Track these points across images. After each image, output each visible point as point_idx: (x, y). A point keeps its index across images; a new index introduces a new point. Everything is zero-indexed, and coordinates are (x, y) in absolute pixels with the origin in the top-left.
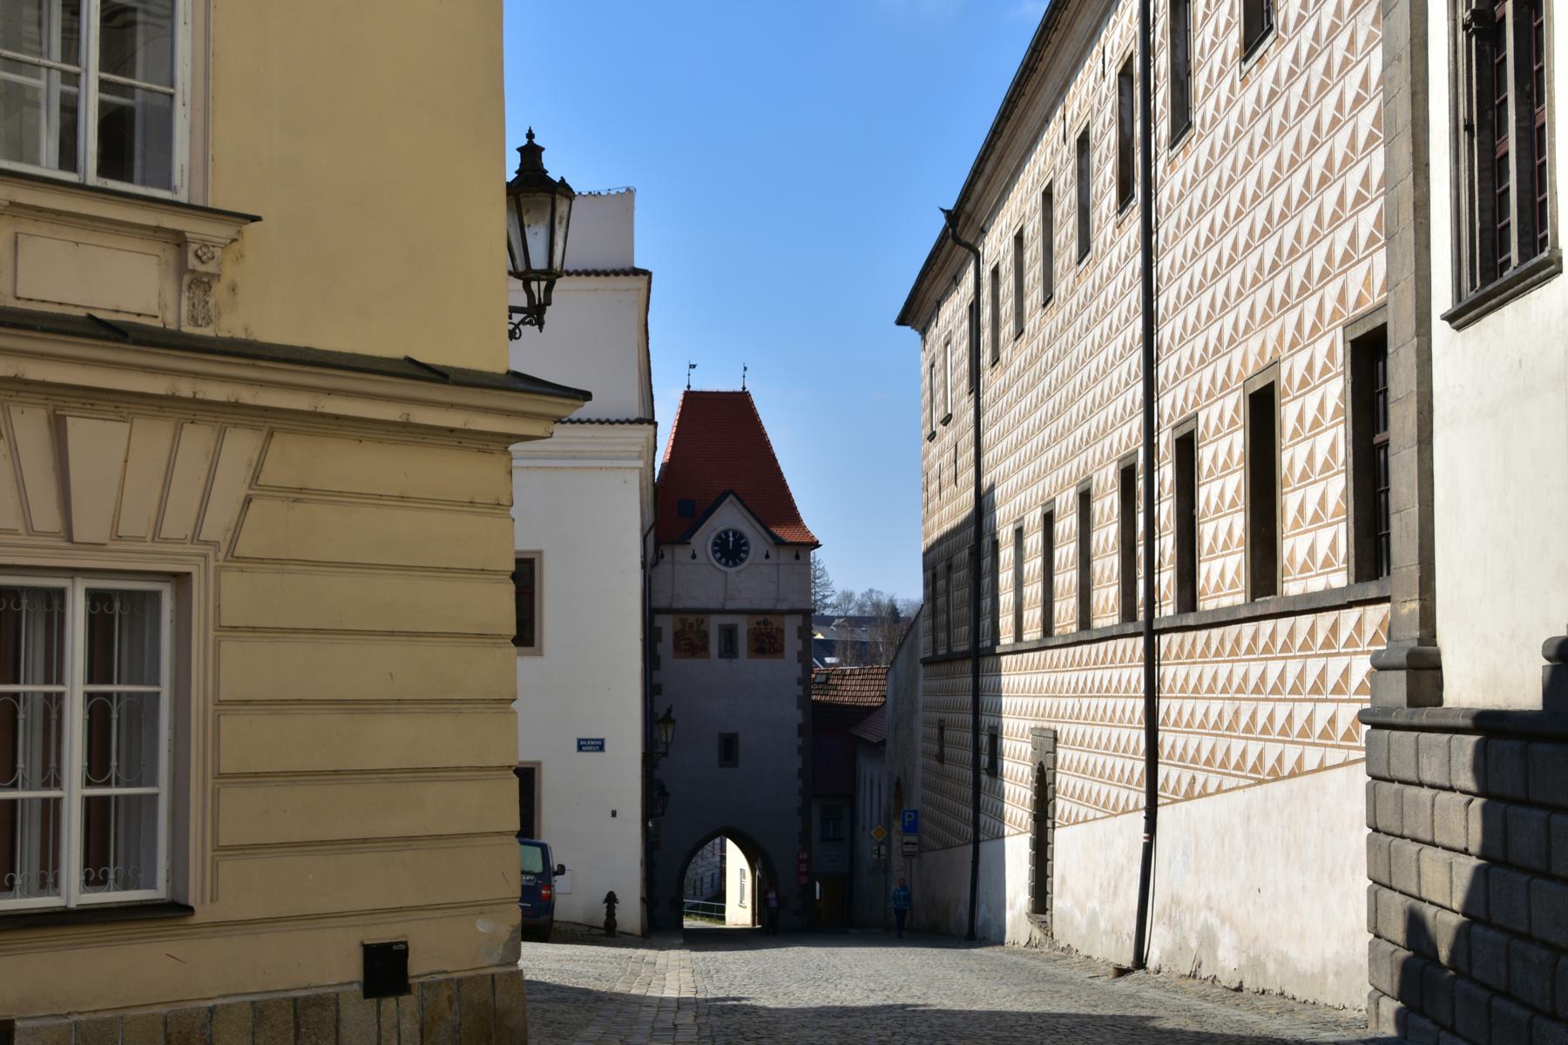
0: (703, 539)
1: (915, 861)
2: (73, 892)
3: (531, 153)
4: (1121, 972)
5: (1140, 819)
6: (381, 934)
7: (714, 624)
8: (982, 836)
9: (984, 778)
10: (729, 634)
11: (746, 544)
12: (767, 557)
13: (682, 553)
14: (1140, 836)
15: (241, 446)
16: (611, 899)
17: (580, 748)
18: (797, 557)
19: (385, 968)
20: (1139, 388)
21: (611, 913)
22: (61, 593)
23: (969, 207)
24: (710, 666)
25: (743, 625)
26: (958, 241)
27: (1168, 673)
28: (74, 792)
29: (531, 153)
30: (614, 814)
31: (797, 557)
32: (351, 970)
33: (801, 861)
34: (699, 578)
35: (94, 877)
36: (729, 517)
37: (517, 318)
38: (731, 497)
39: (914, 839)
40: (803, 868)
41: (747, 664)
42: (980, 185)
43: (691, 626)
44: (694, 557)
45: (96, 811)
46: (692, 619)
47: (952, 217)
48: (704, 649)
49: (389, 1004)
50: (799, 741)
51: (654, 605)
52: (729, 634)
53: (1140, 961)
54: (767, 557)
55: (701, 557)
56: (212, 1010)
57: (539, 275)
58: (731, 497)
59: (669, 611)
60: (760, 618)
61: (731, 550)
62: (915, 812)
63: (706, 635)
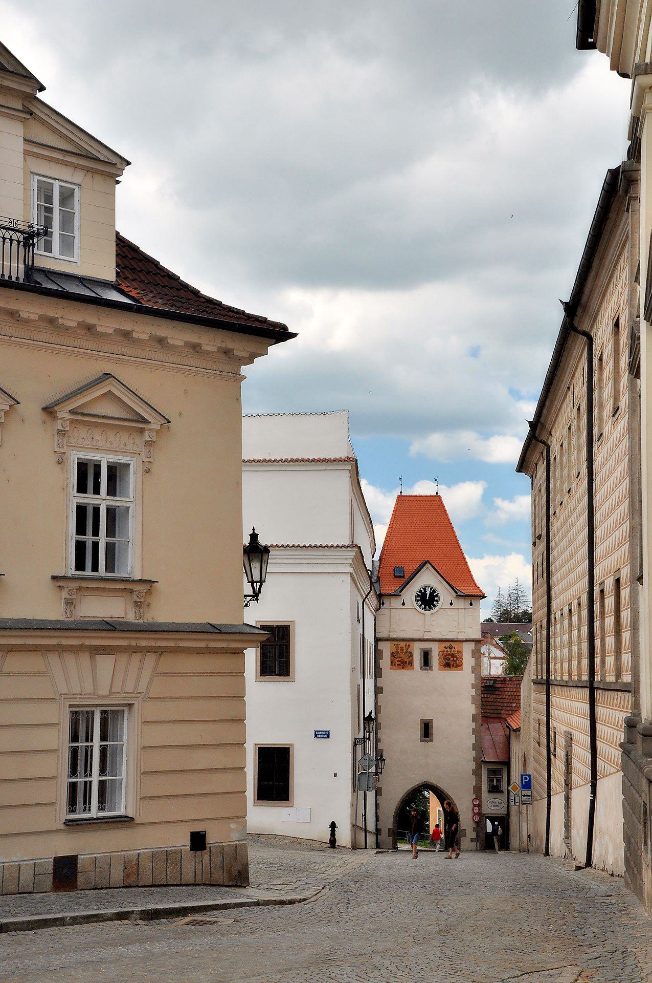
0: (410, 594)
1: (530, 807)
2: (94, 813)
3: (254, 536)
4: (578, 868)
5: (588, 788)
6: (197, 828)
7: (416, 651)
8: (552, 793)
9: (552, 756)
10: (426, 655)
11: (437, 596)
12: (451, 604)
13: (395, 603)
14: (589, 797)
15: (151, 659)
16: (333, 826)
17: (316, 736)
18: (471, 604)
19: (198, 841)
20: (587, 562)
21: (333, 834)
22: (93, 712)
23: (542, 420)
24: (415, 675)
26: (537, 440)
27: (599, 710)
28: (95, 778)
29: (254, 536)
30: (335, 775)
31: (471, 604)
32: (187, 841)
33: (475, 806)
34: (406, 619)
35: (101, 809)
36: (427, 579)
37: (249, 599)
38: (428, 565)
39: (528, 793)
40: (476, 810)
41: (438, 675)
42: (545, 411)
43: (402, 649)
44: (403, 604)
45: (102, 784)
46: (402, 644)
47: (533, 425)
48: (411, 663)
49: (199, 853)
50: (473, 725)
51: (378, 636)
52: (426, 655)
53: (589, 863)
54: (451, 604)
55: (407, 605)
56: (139, 854)
57: (257, 582)
58: (428, 565)
59: (388, 640)
60: (447, 644)
61: (428, 600)
62: (529, 776)
63: (411, 655)
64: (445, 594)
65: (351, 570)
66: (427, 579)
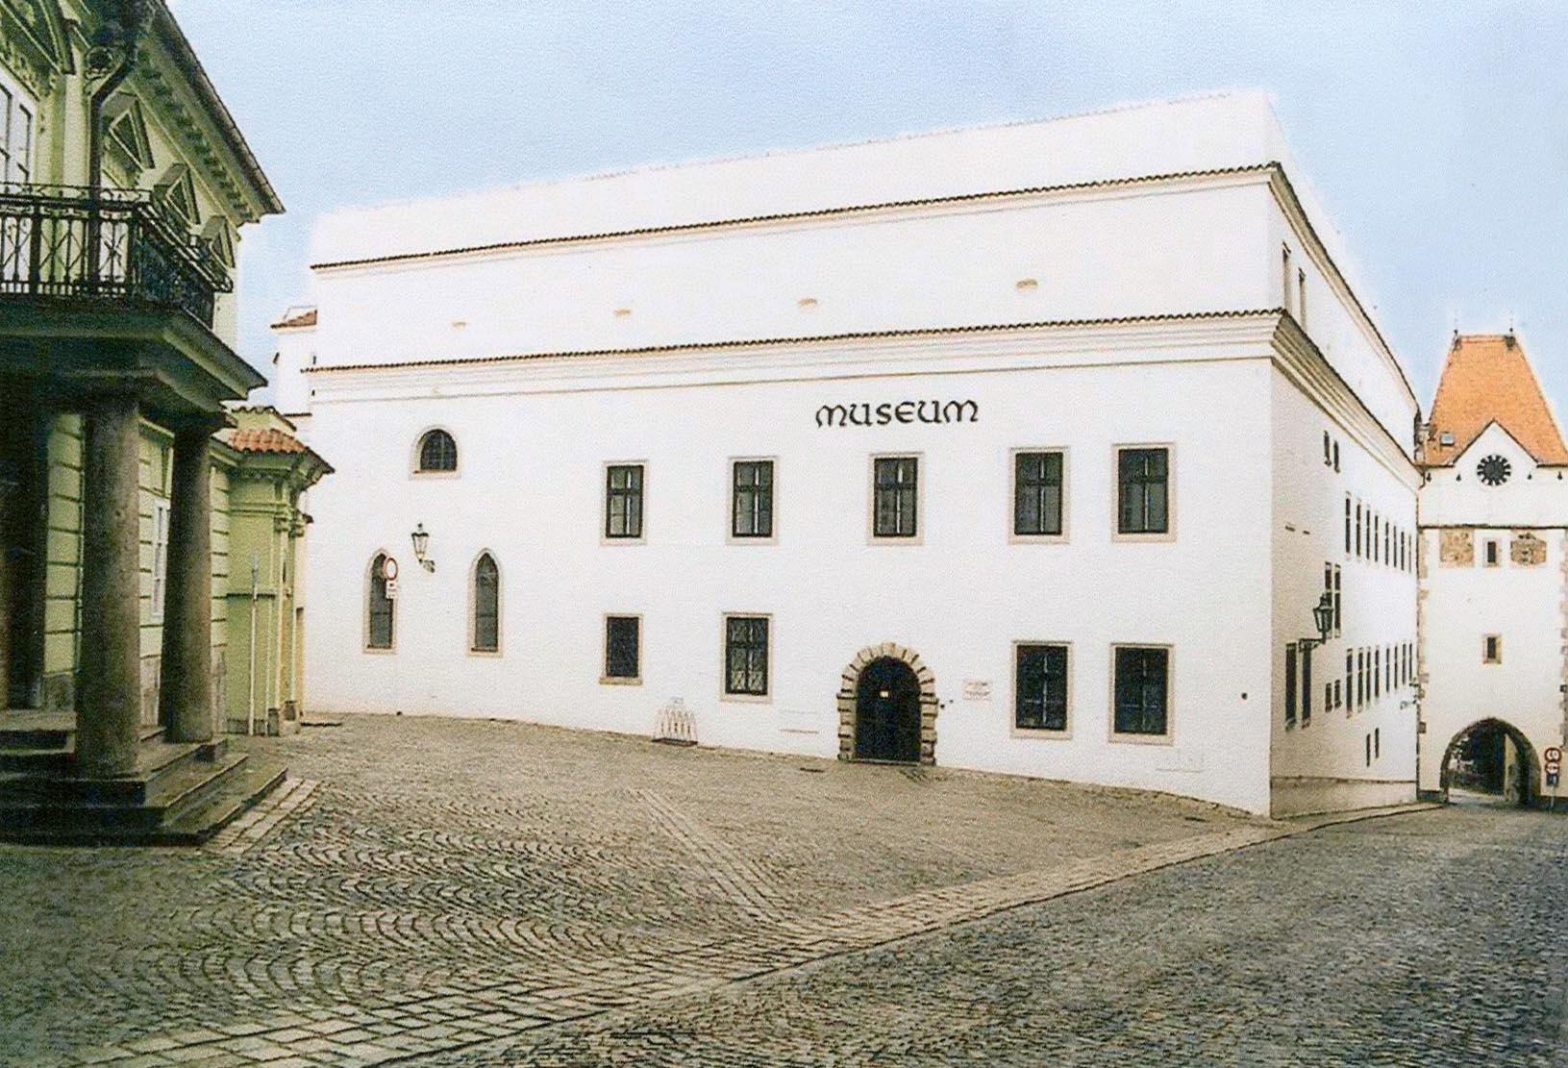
25: (1504, 539)
64: (1520, 463)
65: (1273, 352)
66: (1494, 443)
